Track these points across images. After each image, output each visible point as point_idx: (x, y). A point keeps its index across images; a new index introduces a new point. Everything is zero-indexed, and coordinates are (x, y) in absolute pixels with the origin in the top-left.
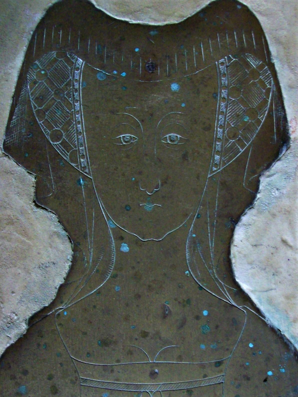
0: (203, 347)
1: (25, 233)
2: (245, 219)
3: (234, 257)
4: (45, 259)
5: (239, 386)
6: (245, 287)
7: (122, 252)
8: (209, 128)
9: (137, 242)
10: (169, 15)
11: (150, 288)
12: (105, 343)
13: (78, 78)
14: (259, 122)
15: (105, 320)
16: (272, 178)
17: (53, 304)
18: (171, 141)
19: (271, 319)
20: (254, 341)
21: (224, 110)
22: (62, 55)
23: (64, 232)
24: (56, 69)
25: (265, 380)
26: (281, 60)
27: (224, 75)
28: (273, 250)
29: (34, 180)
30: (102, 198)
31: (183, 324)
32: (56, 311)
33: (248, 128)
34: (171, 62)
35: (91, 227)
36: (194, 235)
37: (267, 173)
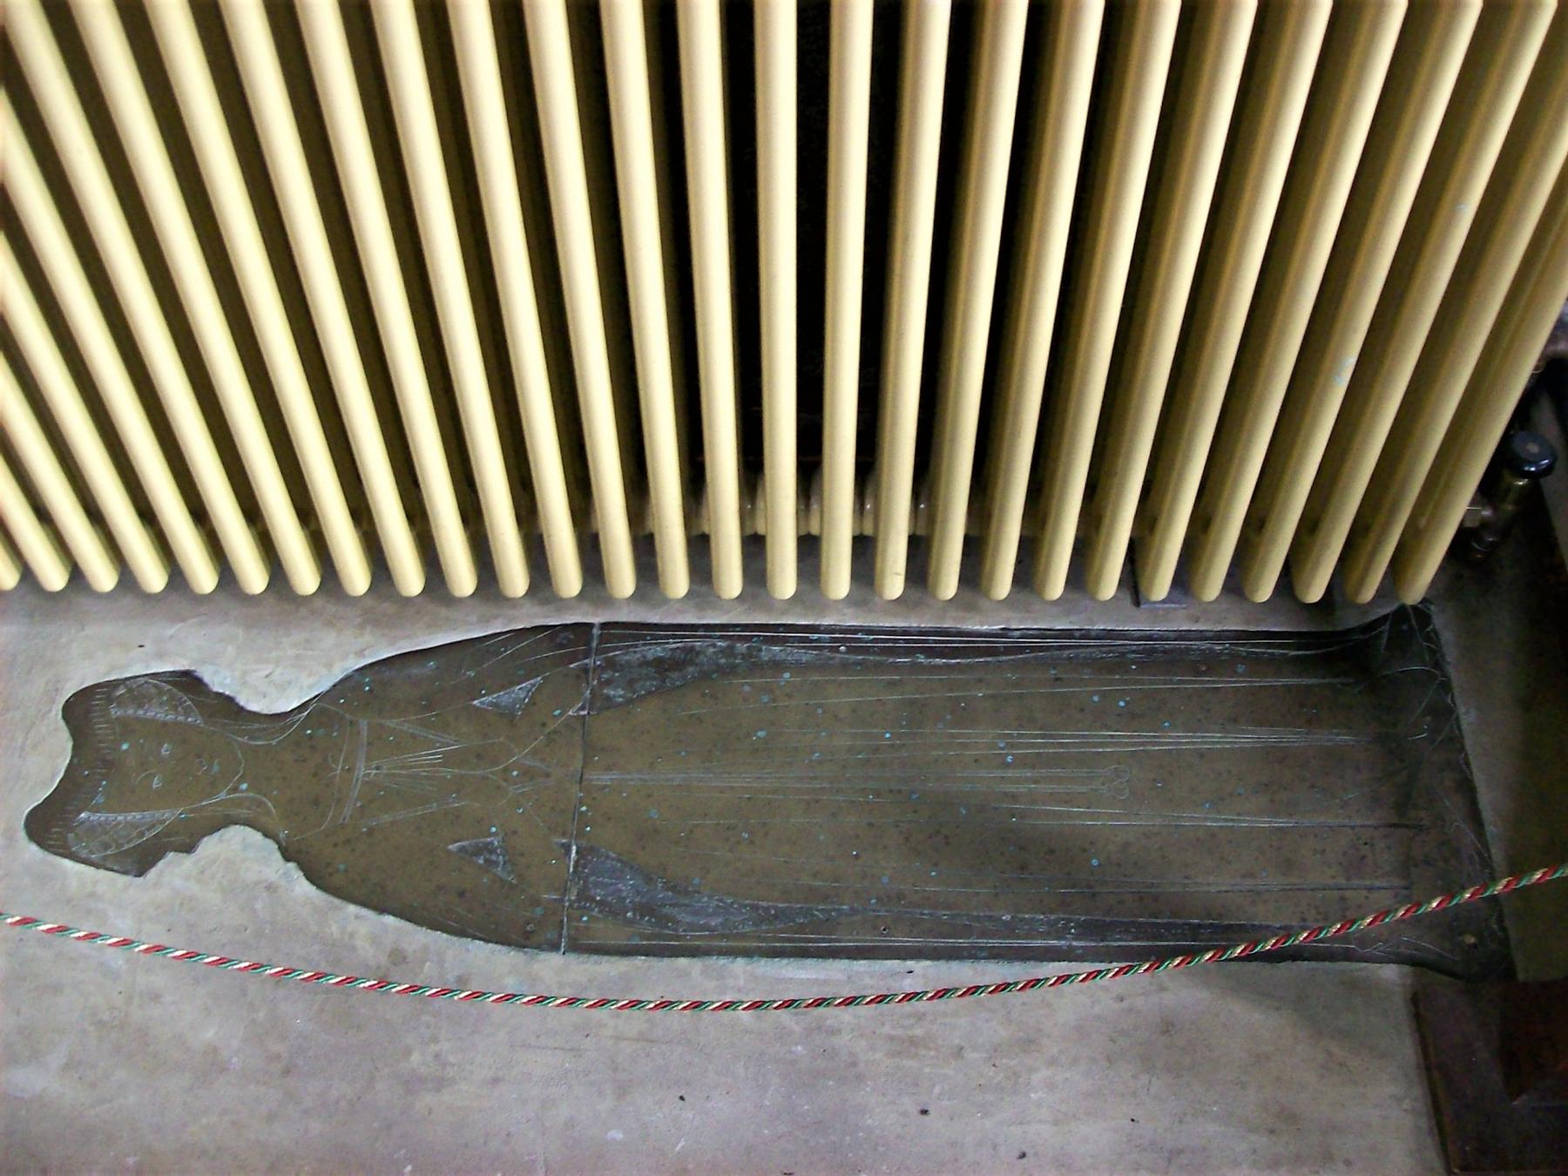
8: (165, 724)
15: (1473, 940)
17: (278, 842)
22: (72, 830)
33: (172, 698)
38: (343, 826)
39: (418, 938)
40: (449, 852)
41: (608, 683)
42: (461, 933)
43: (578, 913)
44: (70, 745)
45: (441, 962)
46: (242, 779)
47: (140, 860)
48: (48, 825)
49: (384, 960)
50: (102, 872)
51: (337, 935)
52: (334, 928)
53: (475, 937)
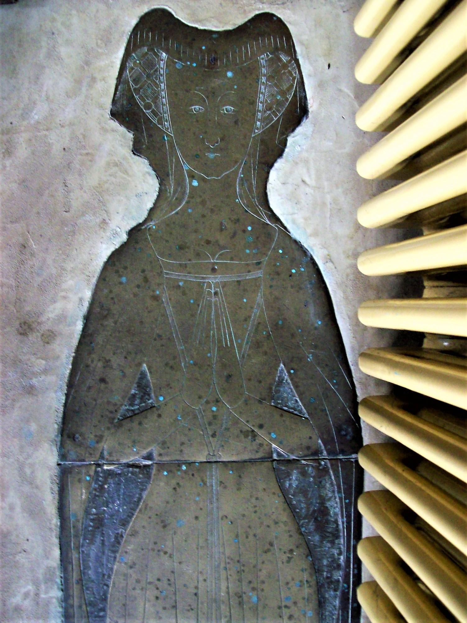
0: (248, 251)
1: (126, 172)
2: (276, 165)
3: (270, 191)
4: (140, 190)
5: (273, 279)
6: (278, 212)
7: (193, 186)
8: (253, 103)
9: (204, 180)
10: (226, 24)
11: (212, 211)
12: (181, 248)
13: (162, 67)
14: (287, 99)
16: (296, 138)
18: (227, 111)
19: (295, 234)
20: (283, 249)
21: (264, 91)
22: (151, 49)
23: (153, 172)
24: (147, 60)
25: (290, 276)
26: (303, 57)
27: (264, 67)
28: (296, 187)
29: (132, 136)
30: (180, 149)
31: (234, 235)
32: (147, 226)
33: (280, 104)
34: (228, 57)
35: (172, 169)
36: (242, 176)
37: (292, 135)
38: (160, 274)
39: (65, 352)
40: (140, 364)
41: (304, 473)
42: (70, 385)
43: (92, 473)
44: (230, 27)
45: (45, 371)
46: (202, 180)
47: (126, 111)
48: (157, 26)
49: (45, 328)
50: (115, 82)
51: (64, 286)
52: (71, 282)
53: (67, 395)
